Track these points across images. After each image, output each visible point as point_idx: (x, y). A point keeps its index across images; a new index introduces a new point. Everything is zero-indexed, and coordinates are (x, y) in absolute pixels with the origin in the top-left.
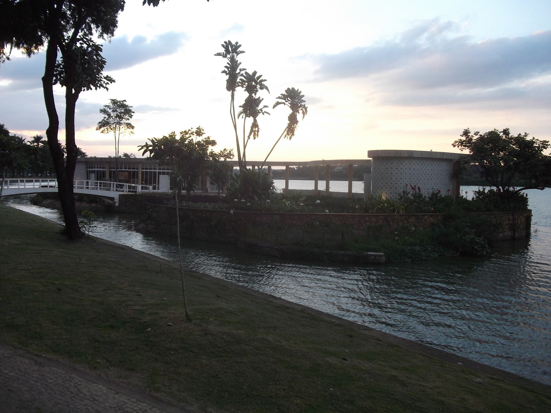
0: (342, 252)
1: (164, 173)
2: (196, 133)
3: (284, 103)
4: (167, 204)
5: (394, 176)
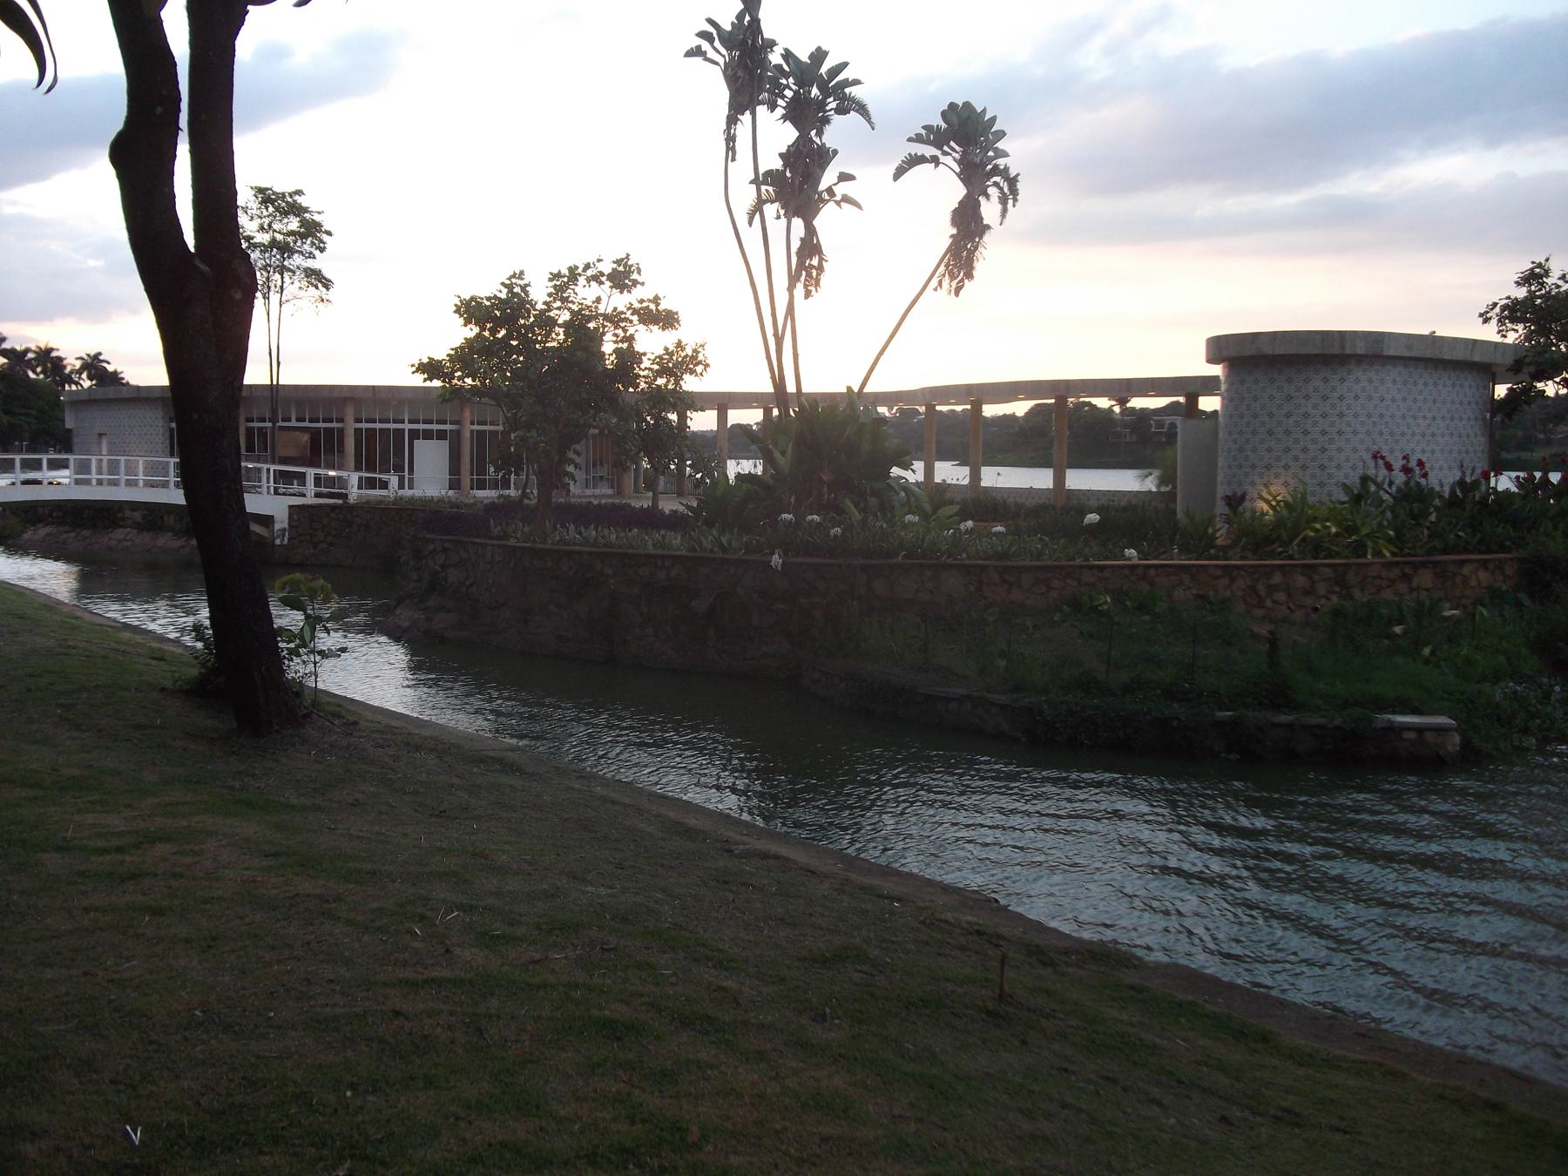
0: (1283, 718)
1: (428, 435)
2: (611, 277)
3: (935, 161)
4: (506, 536)
5: (1315, 424)
